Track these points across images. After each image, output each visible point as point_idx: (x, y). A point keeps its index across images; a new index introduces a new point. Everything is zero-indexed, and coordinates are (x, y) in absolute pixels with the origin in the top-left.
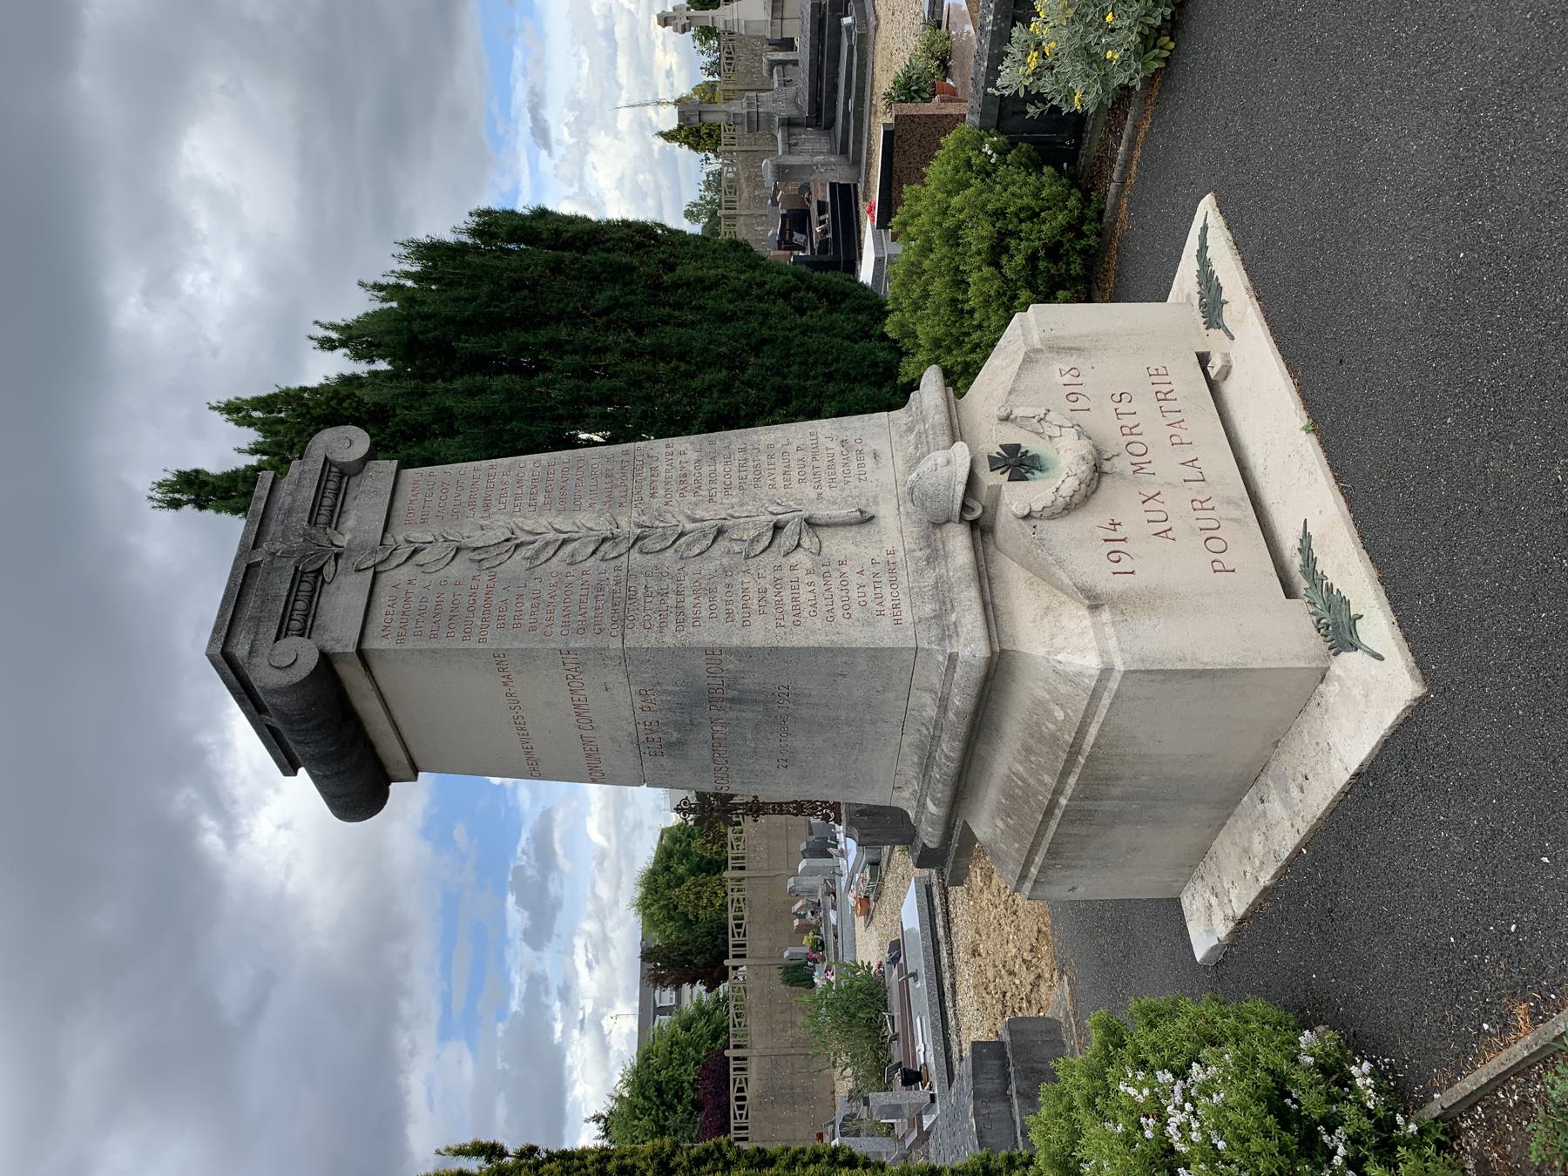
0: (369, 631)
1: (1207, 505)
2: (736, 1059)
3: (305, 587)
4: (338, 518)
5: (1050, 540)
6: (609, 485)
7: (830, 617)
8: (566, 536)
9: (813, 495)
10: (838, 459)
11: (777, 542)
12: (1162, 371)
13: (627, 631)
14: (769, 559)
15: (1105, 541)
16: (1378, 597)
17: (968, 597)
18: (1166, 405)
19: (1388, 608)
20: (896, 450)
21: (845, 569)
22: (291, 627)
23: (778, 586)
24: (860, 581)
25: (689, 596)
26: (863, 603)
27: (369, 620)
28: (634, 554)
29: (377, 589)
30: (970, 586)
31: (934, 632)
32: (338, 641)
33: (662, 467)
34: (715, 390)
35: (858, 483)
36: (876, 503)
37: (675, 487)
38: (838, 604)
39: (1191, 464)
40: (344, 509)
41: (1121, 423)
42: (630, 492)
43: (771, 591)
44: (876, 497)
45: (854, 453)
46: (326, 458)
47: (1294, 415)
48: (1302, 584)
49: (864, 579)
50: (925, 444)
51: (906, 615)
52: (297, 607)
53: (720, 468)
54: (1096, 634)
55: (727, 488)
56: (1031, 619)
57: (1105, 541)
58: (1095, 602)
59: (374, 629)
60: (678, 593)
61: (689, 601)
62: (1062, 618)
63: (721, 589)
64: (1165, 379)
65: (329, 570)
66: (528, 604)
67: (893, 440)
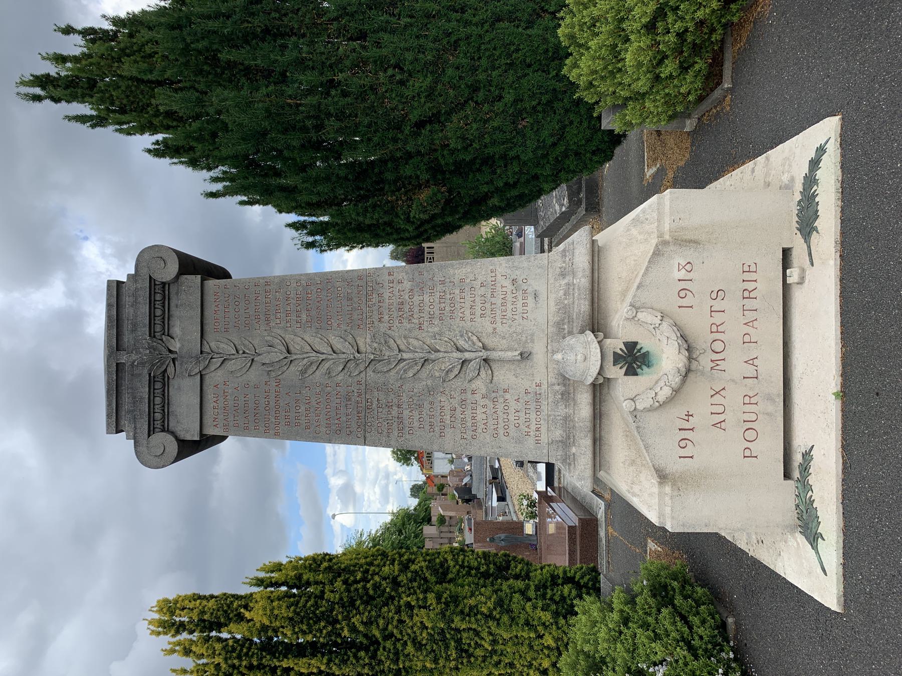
0: (205, 421)
1: (753, 400)
2: (428, 248)
3: (158, 385)
4: (168, 324)
5: (644, 428)
6: (350, 308)
7: (495, 436)
8: (324, 357)
9: (490, 330)
10: (509, 297)
11: (463, 372)
12: (753, 268)
13: (367, 435)
14: (458, 383)
15: (680, 429)
16: (838, 542)
17: (585, 443)
18: (749, 304)
19: (842, 551)
21: (507, 396)
22: (156, 418)
23: (463, 407)
24: (516, 407)
25: (406, 409)
26: (517, 425)
27: (203, 411)
28: (370, 372)
29: (205, 388)
30: (587, 436)
31: (560, 453)
32: (187, 431)
33: (386, 295)
34: (422, 95)
36: (533, 341)
37: (395, 314)
38: (501, 424)
39: (751, 362)
40: (171, 313)
41: (713, 320)
42: (364, 315)
43: (459, 410)
44: (533, 335)
46: (150, 277)
47: (832, 378)
48: (796, 474)
49: (520, 406)
50: (572, 296)
51: (544, 438)
52: (156, 403)
53: (426, 298)
54: (659, 500)
55: (432, 317)
56: (622, 460)
57: (680, 429)
58: (662, 476)
59: (208, 420)
60: (399, 406)
61: (406, 413)
62: (641, 475)
63: (426, 405)
64: (753, 276)
65: (171, 370)
66: (303, 408)
67: (550, 282)
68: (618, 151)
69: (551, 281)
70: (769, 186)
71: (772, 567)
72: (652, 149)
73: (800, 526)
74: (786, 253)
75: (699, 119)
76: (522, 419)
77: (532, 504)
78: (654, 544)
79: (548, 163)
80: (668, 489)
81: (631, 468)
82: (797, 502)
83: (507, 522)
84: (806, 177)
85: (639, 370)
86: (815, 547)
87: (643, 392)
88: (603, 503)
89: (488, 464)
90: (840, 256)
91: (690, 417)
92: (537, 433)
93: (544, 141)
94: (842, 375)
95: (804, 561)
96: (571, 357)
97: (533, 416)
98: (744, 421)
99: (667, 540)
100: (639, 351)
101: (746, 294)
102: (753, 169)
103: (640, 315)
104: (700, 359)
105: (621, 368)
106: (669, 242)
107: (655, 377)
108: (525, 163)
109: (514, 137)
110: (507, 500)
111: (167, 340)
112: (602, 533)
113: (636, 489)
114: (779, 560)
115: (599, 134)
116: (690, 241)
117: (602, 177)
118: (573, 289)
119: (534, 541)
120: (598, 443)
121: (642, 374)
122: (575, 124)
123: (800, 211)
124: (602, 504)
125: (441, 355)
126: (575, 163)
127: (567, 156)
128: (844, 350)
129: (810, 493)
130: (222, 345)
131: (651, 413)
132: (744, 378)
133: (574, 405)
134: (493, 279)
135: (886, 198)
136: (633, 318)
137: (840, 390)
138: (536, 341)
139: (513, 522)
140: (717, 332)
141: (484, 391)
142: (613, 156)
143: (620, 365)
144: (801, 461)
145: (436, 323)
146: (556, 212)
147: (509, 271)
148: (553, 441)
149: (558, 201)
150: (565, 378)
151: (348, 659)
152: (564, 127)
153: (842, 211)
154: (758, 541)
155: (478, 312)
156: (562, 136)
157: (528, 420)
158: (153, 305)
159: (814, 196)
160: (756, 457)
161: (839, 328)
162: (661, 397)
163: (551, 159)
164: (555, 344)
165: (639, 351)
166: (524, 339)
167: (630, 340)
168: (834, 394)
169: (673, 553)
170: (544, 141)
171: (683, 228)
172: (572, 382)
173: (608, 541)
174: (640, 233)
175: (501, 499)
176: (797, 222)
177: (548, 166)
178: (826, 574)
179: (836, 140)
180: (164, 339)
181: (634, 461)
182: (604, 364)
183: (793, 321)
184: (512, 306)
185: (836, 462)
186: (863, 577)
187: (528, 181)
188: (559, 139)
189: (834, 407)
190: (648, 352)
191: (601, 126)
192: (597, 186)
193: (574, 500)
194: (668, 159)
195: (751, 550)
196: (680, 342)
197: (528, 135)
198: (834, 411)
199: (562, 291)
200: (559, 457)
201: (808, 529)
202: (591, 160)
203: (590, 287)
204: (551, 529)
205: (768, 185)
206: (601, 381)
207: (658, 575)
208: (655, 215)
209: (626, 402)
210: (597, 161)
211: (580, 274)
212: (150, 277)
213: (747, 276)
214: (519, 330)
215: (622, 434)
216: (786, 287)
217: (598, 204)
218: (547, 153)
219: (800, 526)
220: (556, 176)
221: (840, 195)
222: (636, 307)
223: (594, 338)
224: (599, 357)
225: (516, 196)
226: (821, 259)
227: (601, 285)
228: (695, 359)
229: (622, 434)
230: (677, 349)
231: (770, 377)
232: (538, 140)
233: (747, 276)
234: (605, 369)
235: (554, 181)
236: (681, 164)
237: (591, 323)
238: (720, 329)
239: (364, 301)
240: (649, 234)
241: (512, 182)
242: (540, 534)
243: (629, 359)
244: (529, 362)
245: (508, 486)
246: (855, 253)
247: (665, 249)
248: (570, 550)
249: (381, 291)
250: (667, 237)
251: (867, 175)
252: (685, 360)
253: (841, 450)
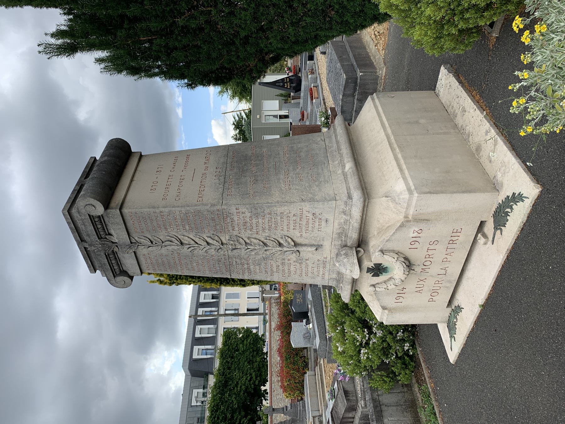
4: (107, 229)
10: (311, 221)
21: (307, 262)
27: (140, 264)
33: (236, 219)
36: (323, 240)
37: (242, 227)
43: (281, 266)
44: (324, 238)
45: (318, 219)
46: (89, 215)
61: (252, 267)
74: (482, 224)
97: (321, 269)
105: (370, 274)
110: (315, 60)
111: (109, 237)
125: (270, 248)
130: (142, 240)
134: (301, 213)
140: (429, 257)
141: (295, 259)
145: (266, 232)
147: (311, 209)
148: (331, 278)
151: (230, 282)
155: (292, 227)
158: (95, 224)
180: (107, 237)
184: (312, 225)
208: (405, 205)
212: (89, 215)
214: (316, 235)
221: (520, 229)
239: (222, 221)
249: (232, 217)
253: (474, 323)
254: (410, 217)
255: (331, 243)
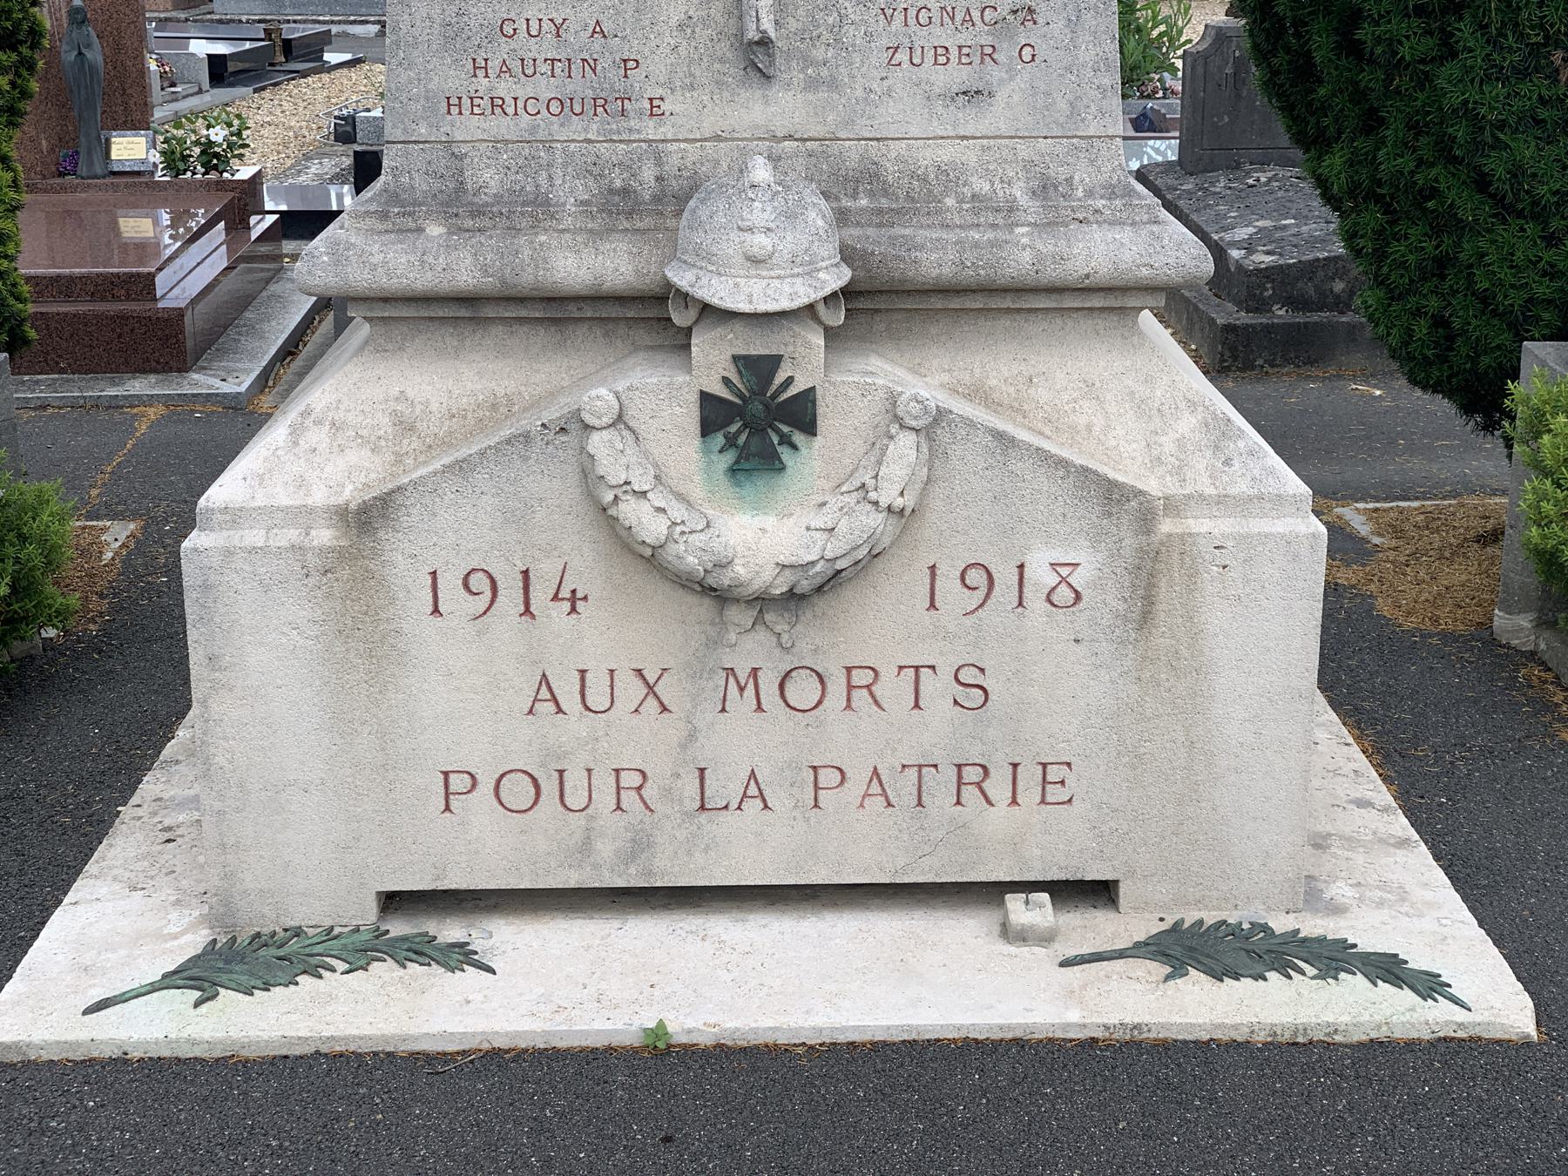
5: (526, 459)
12: (1055, 793)
15: (526, 573)
16: (194, 1043)
18: (941, 786)
20: (983, 149)
24: (573, 25)
26: (508, 30)
30: (486, 273)
31: (421, 184)
35: (885, 42)
36: (812, 85)
41: (888, 672)
44: (833, 84)
45: (989, 40)
47: (712, 1021)
48: (398, 928)
49: (577, 38)
50: (970, 219)
51: (467, 127)
56: (410, 393)
57: (526, 573)
64: (1029, 793)
67: (1021, 146)
68: (1442, 407)
69: (1024, 150)
70: (1317, 846)
71: (91, 867)
72: (1431, 522)
73: (234, 939)
75: (1533, 653)
76: (532, 49)
77: (213, 158)
78: (122, 538)
79: (1420, 162)
80: (324, 536)
81: (385, 420)
82: (311, 932)
83: (144, 89)
84: (1344, 945)
85: (719, 439)
86: (171, 981)
87: (646, 454)
88: (243, 389)
89: (335, 29)
90: (1094, 1040)
91: (567, 606)
92: (486, 103)
93: (1498, 145)
94: (720, 1046)
95: (123, 952)
96: (760, 213)
97: (545, 88)
98: (561, 772)
99: (140, 577)
100: (787, 441)
101: (972, 774)
102: (1371, 805)
103: (906, 441)
104: (761, 635)
105: (726, 381)
106: (1148, 532)
107: (697, 492)
108: (1424, 80)
109: (1521, 37)
112: (139, 386)
113: (317, 437)
114: (117, 887)
115: (1505, 338)
116: (1149, 601)
117: (1339, 377)
118: (994, 226)
119: (91, 163)
120: (463, 313)
121: (706, 451)
122: (1548, 256)
123: (1235, 931)
124: (239, 384)
126: (1411, 257)
127: (1436, 231)
128: (800, 1050)
129: (341, 966)
131: (574, 479)
132: (702, 770)
133: (591, 231)
135: (1279, 1158)
136: (897, 419)
137: (673, 1041)
138: (810, 97)
139: (146, 108)
142: (1424, 388)
143: (735, 379)
144: (440, 940)
146: (1225, 229)
148: (460, 158)
149: (1264, 236)
150: (682, 199)
152: (1539, 213)
153: (1234, 1045)
154: (169, 829)
156: (1510, 208)
157: (527, 67)
159: (1285, 969)
160: (447, 808)
161: (867, 1037)
162: (632, 512)
163: (1434, 172)
164: (801, 164)
165: (787, 441)
166: (819, 53)
167: (821, 410)
168: (661, 1024)
169: (101, 596)
170: (1498, 145)
171: (1193, 575)
172: (671, 223)
173: (114, 405)
174: (1181, 443)
175: (219, 70)
176: (1201, 922)
177: (1407, 163)
178: (88, 1011)
179: (1460, 1025)
181: (412, 429)
182: (738, 326)
183: (885, 915)
185: (444, 1035)
186: (92, 1110)
187: (1359, 95)
188: (1498, 199)
189: (620, 1026)
190: (783, 468)
191: (1533, 339)
192: (1310, 362)
193: (244, 302)
194: (1400, 568)
195: (139, 812)
196: (818, 568)
197: (1524, 88)
198: (608, 1026)
199: (987, 187)
200: (405, 179)
201: (227, 962)
202: (1418, 313)
203: (1002, 282)
204: (135, 226)
205: (1319, 843)
206: (680, 318)
207: (23, 539)
208: (1242, 487)
209: (611, 397)
210: (1410, 333)
211: (1046, 246)
213: (1029, 777)
214: (851, 34)
215: (501, 391)
216: (991, 893)
217: (1248, 366)
218: (1456, 160)
219: (234, 939)
220: (1372, 196)
221: (1287, 1037)
222: (933, 428)
223: (828, 291)
224: (762, 307)
225: (1308, 56)
226: (1084, 987)
227: (1005, 322)
228: (759, 621)
229: (501, 391)
230: (793, 560)
231: (707, 849)
232: (1502, 125)
233: (1029, 777)
234: (720, 331)
235: (1352, 192)
236: (1384, 607)
237: (877, 285)
238: (860, 696)
240: (1179, 471)
241: (1360, 35)
242: (115, 188)
243: (757, 408)
244: (733, 71)
245: (267, 94)
246: (1106, 1079)
247: (1125, 519)
248: (71, 279)
250: (1166, 526)
251: (1350, 1108)
252: (757, 585)
253: (486, 1046)
254: (1166, 526)
255: (785, 138)
